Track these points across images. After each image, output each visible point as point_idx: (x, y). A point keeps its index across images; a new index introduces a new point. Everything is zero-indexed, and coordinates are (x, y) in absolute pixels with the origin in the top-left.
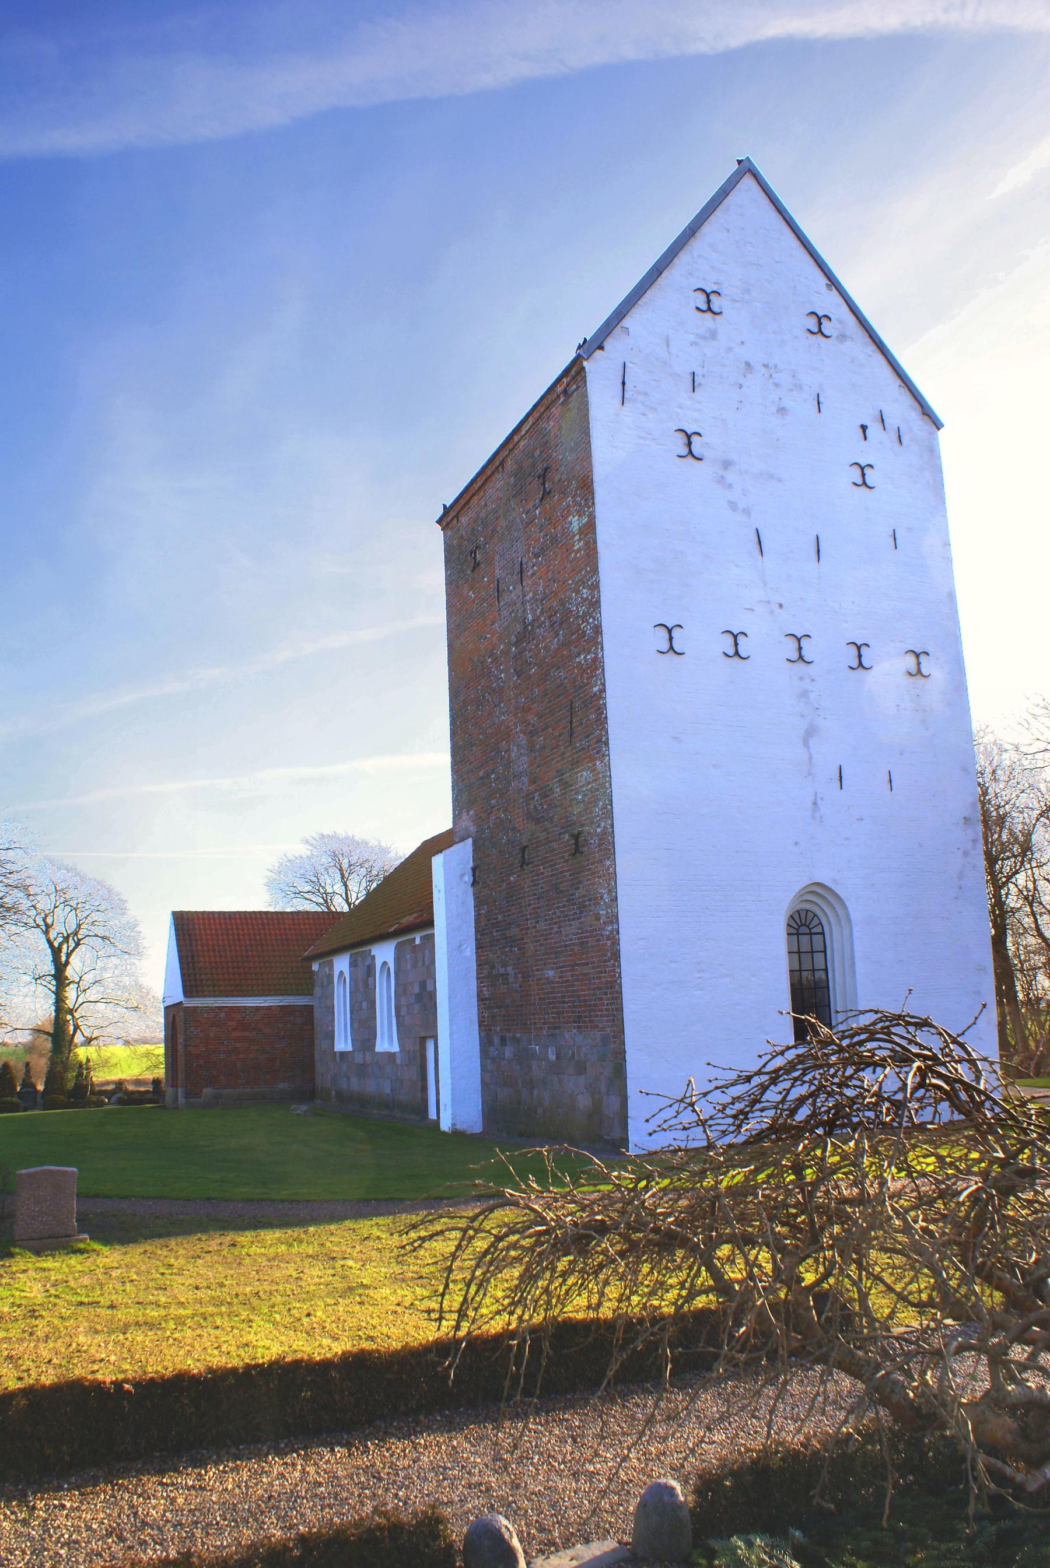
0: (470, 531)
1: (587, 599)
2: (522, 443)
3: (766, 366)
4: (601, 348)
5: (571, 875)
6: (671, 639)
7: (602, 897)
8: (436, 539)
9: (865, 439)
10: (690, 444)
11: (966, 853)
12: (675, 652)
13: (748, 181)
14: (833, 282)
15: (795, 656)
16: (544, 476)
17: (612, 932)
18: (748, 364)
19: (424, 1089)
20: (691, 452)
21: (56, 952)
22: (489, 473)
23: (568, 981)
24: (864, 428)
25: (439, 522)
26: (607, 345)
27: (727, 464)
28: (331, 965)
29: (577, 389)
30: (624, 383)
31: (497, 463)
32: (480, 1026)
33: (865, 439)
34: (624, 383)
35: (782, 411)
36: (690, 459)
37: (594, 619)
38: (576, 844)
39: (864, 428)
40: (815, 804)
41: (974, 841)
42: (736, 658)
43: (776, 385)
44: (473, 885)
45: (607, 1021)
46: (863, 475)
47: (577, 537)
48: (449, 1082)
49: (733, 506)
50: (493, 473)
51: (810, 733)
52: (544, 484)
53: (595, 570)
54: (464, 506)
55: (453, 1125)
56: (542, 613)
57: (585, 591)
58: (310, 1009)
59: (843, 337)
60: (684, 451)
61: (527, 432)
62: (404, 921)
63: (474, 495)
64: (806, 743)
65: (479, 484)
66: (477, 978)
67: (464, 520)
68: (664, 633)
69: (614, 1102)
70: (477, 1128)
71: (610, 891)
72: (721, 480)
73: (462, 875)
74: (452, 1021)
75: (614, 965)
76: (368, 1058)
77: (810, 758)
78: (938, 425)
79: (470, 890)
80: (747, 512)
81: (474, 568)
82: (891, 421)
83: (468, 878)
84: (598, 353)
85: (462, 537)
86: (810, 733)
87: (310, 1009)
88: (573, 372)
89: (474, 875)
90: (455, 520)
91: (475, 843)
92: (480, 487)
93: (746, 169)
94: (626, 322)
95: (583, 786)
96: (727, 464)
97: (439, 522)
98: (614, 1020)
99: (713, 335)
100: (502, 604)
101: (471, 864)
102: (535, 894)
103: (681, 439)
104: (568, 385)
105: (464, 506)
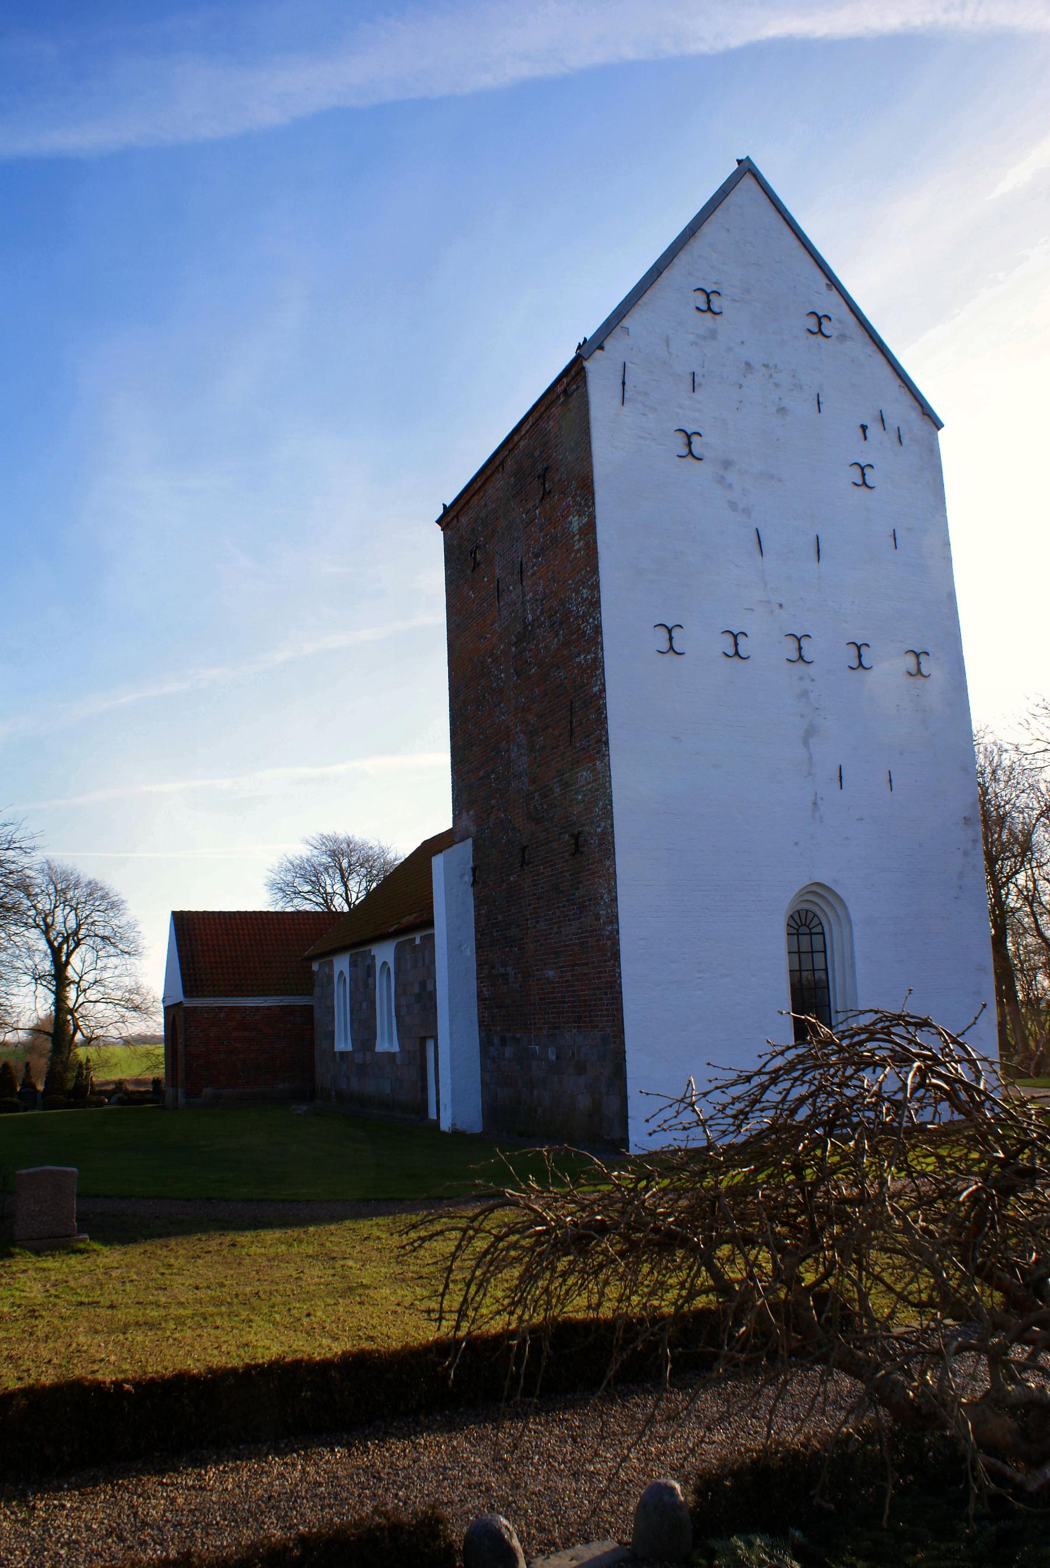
2: (522, 443)
3: (766, 366)
4: (601, 348)
5: (571, 875)
7: (602, 897)
8: (437, 537)
9: (865, 439)
10: (689, 444)
11: (966, 854)
12: (675, 652)
13: (748, 181)
14: (833, 282)
17: (612, 932)
19: (425, 1089)
20: (691, 452)
21: (56, 952)
22: (489, 473)
23: (568, 981)
24: (864, 428)
25: (439, 522)
26: (607, 345)
27: (727, 464)
28: (331, 965)
30: (624, 383)
31: (498, 463)
33: (701, 459)
34: (624, 383)
35: (782, 411)
37: (594, 619)
39: (864, 428)
40: (815, 804)
41: (974, 841)
42: (737, 658)
43: (776, 385)
44: (473, 885)
46: (863, 475)
47: (577, 537)
49: (733, 505)
51: (810, 733)
56: (542, 613)
57: (585, 591)
58: (309, 1009)
59: (843, 337)
60: (684, 451)
61: (527, 432)
63: (474, 494)
64: (806, 743)
65: (479, 484)
67: (464, 520)
71: (610, 891)
72: (721, 480)
73: (463, 875)
75: (614, 965)
77: (810, 758)
78: (938, 425)
79: (471, 890)
80: (747, 512)
81: (474, 568)
82: (891, 421)
83: (468, 878)
84: (598, 353)
86: (810, 733)
87: (309, 1009)
89: (474, 875)
91: (475, 843)
92: (480, 488)
93: (746, 169)
94: (626, 322)
96: (727, 464)
97: (439, 522)
99: (713, 335)
100: (502, 604)
101: (471, 864)
102: (535, 894)
103: (681, 439)
104: (568, 385)
105: (464, 505)
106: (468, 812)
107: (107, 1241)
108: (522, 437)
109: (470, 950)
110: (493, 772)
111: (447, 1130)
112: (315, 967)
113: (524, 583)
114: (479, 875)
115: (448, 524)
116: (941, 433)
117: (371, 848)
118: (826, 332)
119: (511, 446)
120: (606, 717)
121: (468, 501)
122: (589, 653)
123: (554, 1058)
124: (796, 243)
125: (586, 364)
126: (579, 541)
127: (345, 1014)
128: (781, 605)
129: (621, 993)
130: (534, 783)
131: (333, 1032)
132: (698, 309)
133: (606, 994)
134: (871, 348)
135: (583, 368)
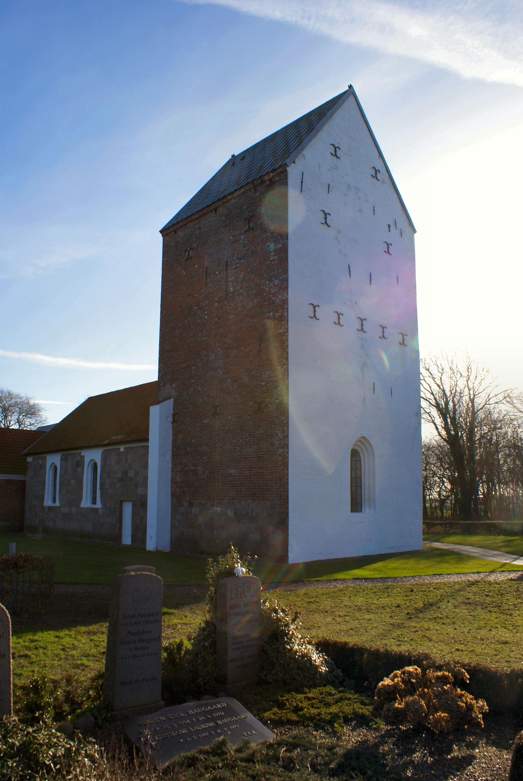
0: (187, 240)
1: (278, 285)
2: (233, 201)
3: (356, 188)
5: (253, 422)
6: (315, 311)
7: (276, 435)
8: (159, 239)
9: (329, 226)
10: (326, 218)
12: (316, 318)
13: (351, 98)
15: (360, 328)
16: (250, 220)
17: (283, 452)
18: (349, 185)
19: (121, 528)
20: (326, 222)
22: (205, 212)
23: (246, 476)
24: (389, 226)
25: (161, 232)
28: (45, 459)
29: (279, 180)
30: (302, 182)
31: (213, 208)
32: (172, 496)
33: (329, 226)
34: (302, 182)
35: (361, 211)
36: (325, 226)
37: (283, 296)
38: (259, 407)
39: (389, 226)
40: (364, 399)
42: (338, 325)
44: (173, 423)
45: (275, 497)
46: (388, 248)
47: (273, 254)
48: (155, 525)
50: (208, 212)
52: (249, 223)
53: (286, 271)
54: (182, 226)
55: (157, 547)
56: (241, 288)
57: (276, 281)
58: (23, 483)
59: (383, 182)
60: (324, 221)
61: (238, 195)
62: (114, 438)
63: (191, 221)
65: (196, 216)
66: (172, 472)
67: (181, 233)
68: (312, 308)
69: (278, 538)
70: (168, 550)
71: (283, 432)
73: (168, 417)
74: (101, 497)
75: (283, 469)
76: (74, 510)
79: (171, 425)
81: (187, 259)
83: (170, 419)
84: (293, 164)
85: (178, 242)
87: (23, 483)
88: (278, 171)
89: (174, 418)
90: (174, 233)
91: (175, 401)
92: (197, 219)
95: (267, 378)
97: (161, 232)
98: (281, 497)
100: (209, 280)
101: (172, 412)
102: (223, 430)
103: (322, 215)
104: (273, 176)
105: (182, 226)
106: (171, 384)
107: (177, 606)
108: (234, 197)
109: (169, 457)
110: (193, 365)
111: (152, 549)
112: (29, 459)
113: (228, 272)
114: (177, 418)
115: (167, 234)
116: (415, 235)
117: (21, 398)
118: (378, 178)
119: (224, 201)
120: (288, 346)
121: (186, 224)
122: (277, 312)
123: (232, 514)
124: (368, 133)
125: (289, 169)
126: (274, 256)
127: (55, 486)
128: (356, 303)
129: (288, 483)
130: (227, 374)
131: (44, 496)
132: (331, 154)
133: (276, 483)
134: (393, 190)
135: (286, 171)
